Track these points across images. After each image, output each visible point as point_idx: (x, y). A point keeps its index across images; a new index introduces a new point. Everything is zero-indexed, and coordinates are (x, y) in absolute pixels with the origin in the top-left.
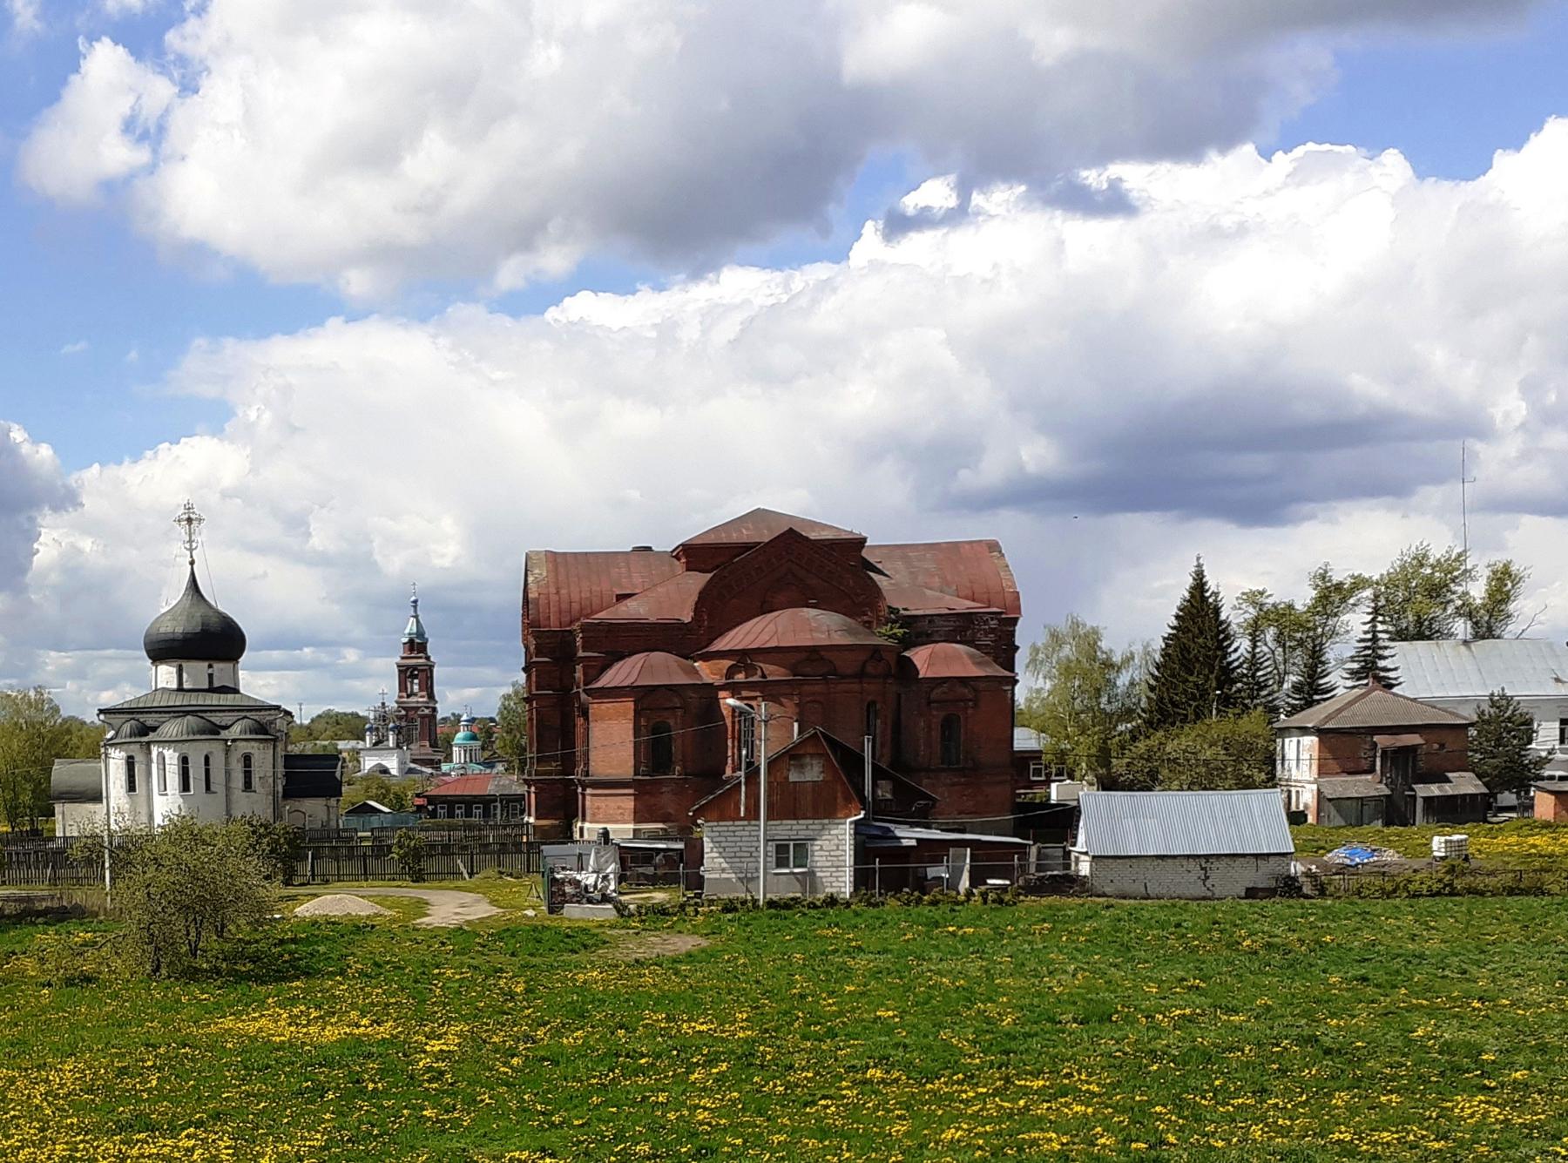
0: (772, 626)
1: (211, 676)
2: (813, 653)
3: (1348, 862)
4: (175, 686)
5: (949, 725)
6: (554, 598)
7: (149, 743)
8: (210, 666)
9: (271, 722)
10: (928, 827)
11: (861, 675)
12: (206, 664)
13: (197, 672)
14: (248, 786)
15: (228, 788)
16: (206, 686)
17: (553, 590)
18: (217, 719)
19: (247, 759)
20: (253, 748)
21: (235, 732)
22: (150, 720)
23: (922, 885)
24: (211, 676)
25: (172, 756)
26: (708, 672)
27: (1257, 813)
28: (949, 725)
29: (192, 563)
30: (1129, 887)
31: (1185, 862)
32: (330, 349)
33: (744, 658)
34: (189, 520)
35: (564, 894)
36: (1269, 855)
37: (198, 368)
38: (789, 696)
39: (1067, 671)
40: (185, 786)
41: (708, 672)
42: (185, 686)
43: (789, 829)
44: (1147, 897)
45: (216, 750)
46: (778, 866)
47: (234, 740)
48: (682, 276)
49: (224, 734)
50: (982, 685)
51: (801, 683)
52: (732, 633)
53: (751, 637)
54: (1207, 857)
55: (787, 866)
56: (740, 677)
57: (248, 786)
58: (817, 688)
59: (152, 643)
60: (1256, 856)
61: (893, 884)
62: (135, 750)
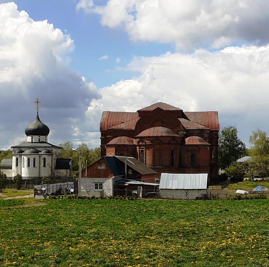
0: (149, 131)
1: (39, 139)
2: (157, 138)
3: (256, 191)
4: (31, 141)
5: (193, 156)
6: (106, 122)
7: (21, 155)
8: (39, 137)
9: (52, 150)
10: (141, 181)
11: (169, 143)
12: (38, 136)
13: (36, 138)
14: (44, 166)
15: (40, 166)
16: (38, 141)
17: (106, 121)
18: (39, 149)
19: (45, 159)
20: (46, 157)
21: (42, 152)
22: (23, 149)
23: (130, 194)
24: (39, 139)
25: (26, 158)
26: (135, 142)
27: (201, 179)
28: (193, 156)
29: (38, 112)
30: (169, 196)
31: (182, 191)
32: (170, 60)
33: (142, 139)
34: (38, 102)
35: (38, 193)
36: (201, 189)
37: (134, 64)
38: (151, 148)
39: (257, 143)
40: (29, 165)
41: (135, 142)
42: (33, 141)
43: (98, 180)
44: (174, 199)
45: (37, 157)
46: (96, 189)
47: (41, 155)
48: (245, 45)
49: (40, 153)
50: (200, 147)
51: (154, 145)
52: (143, 132)
53: (144, 134)
54: (187, 190)
55: (98, 189)
56: (141, 143)
57: (44, 166)
58: (158, 146)
59: (26, 130)
60: (199, 190)
61: (122, 194)
62: (18, 156)
